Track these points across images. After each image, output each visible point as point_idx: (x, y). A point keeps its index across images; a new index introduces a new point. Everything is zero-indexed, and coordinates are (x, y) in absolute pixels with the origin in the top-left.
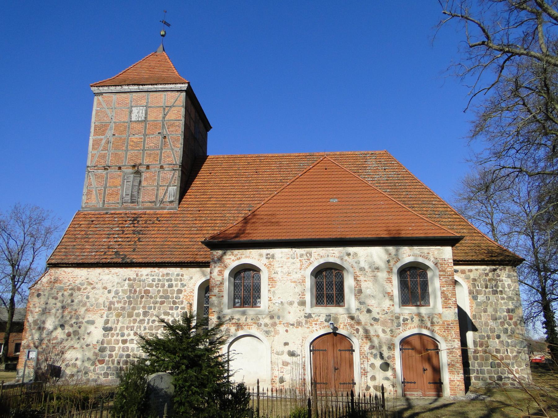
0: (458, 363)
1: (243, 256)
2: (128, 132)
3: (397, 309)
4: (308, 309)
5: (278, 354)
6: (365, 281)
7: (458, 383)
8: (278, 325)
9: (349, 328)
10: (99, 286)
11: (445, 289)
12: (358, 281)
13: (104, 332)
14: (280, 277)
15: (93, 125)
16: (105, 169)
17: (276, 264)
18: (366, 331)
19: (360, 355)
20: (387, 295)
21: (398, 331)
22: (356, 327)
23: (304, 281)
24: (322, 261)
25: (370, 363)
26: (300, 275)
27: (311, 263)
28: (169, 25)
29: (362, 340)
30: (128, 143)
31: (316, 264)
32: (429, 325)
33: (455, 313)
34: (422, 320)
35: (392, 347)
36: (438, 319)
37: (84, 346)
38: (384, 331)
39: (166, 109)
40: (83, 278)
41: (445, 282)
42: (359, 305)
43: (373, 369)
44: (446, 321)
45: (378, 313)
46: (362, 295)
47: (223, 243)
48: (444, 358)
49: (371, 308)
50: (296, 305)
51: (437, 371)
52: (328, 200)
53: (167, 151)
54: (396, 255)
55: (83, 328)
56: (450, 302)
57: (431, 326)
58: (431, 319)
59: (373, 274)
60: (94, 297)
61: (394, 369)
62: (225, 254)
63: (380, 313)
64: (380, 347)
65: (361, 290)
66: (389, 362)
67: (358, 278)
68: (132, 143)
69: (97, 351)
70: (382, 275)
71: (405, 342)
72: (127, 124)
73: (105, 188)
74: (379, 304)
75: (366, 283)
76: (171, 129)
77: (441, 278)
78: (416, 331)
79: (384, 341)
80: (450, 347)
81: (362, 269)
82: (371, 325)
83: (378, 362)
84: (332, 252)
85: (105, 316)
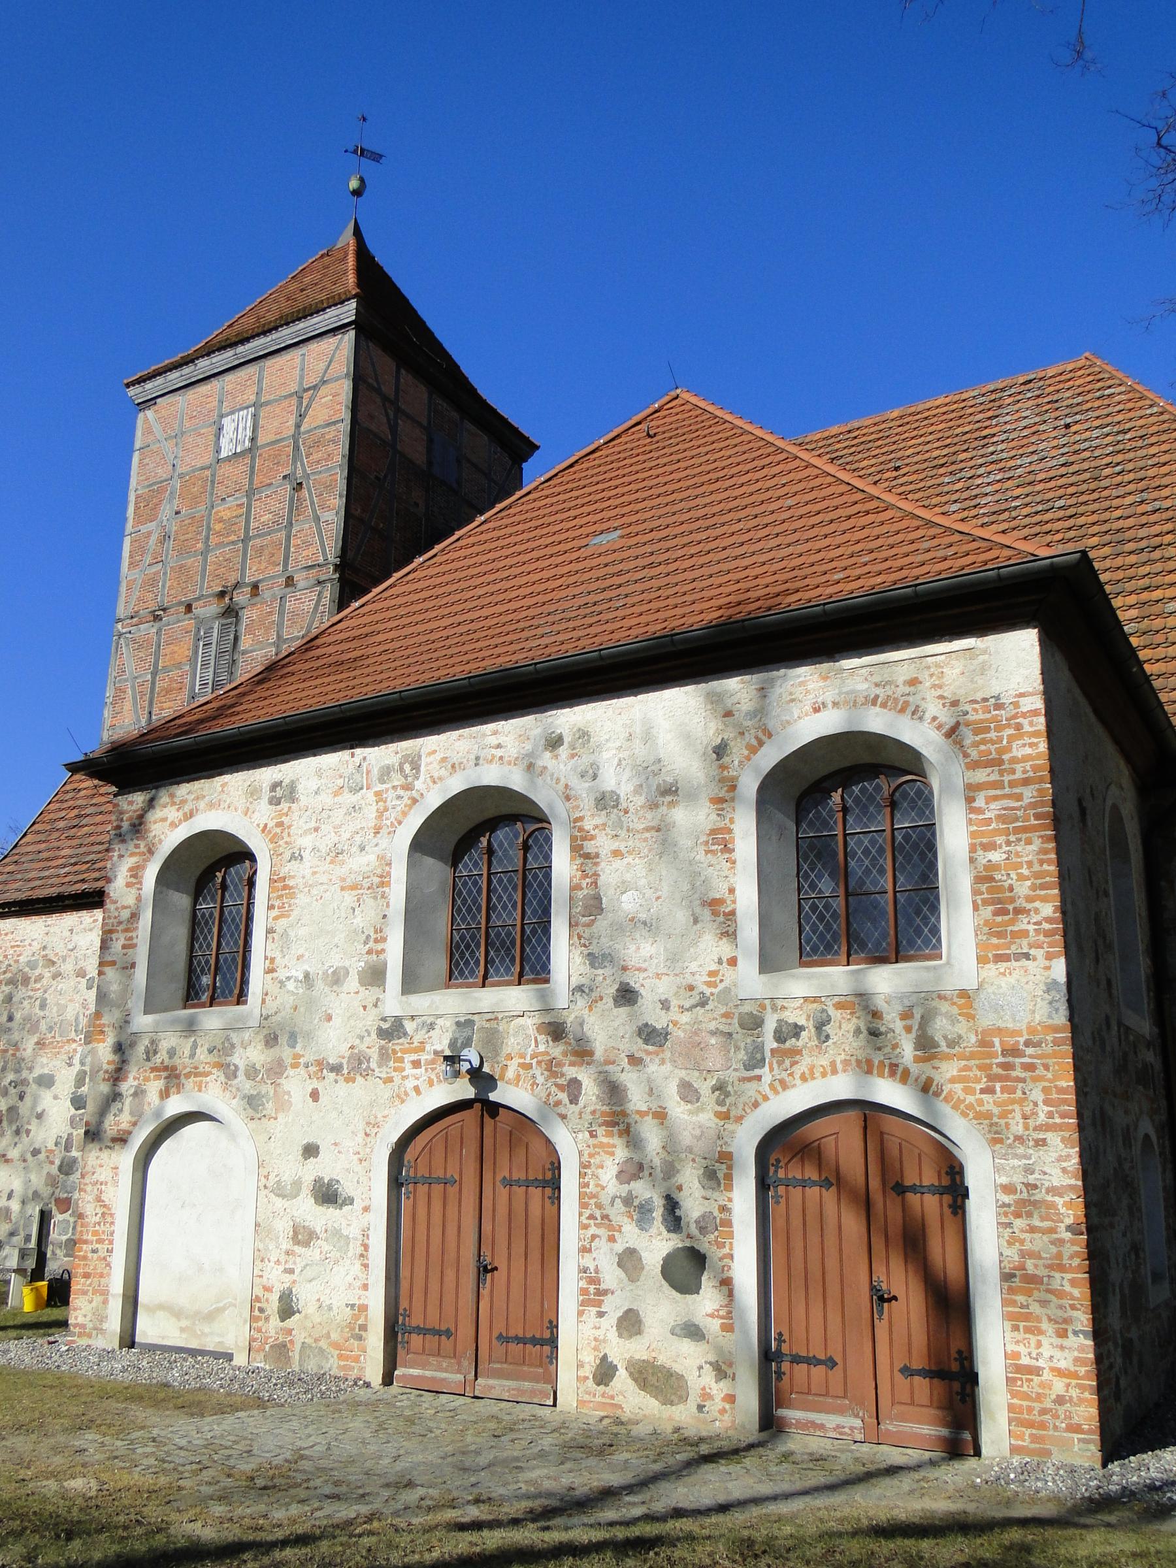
0: (1061, 1268)
1: (202, 804)
2: (212, 494)
3: (749, 980)
4: (393, 1001)
5: (280, 1191)
6: (617, 853)
7: (1059, 1386)
8: (291, 1072)
9: (540, 1080)
10: (68, 967)
11: (996, 856)
12: (587, 856)
13: (73, 1111)
14: (308, 873)
15: (132, 497)
16: (157, 618)
17: (299, 822)
18: (613, 1091)
19: (583, 1205)
20: (706, 913)
21: (751, 1089)
22: (571, 1072)
23: (384, 881)
24: (456, 785)
25: (619, 1247)
26: (372, 858)
27: (415, 801)
28: (377, 157)
29: (593, 1135)
30: (209, 528)
31: (434, 800)
32: (908, 1051)
33: (1051, 986)
34: (874, 1033)
35: (721, 1170)
36: (954, 1021)
37: (29, 1156)
38: (688, 1092)
39: (303, 396)
40: (36, 946)
41: (1000, 818)
42: (586, 969)
43: (633, 1279)
44: (1000, 1031)
45: (665, 1005)
46: (602, 924)
47: (146, 765)
48: (988, 1239)
49: (635, 980)
50: (352, 982)
51: (951, 1307)
52: (583, 542)
53: (304, 527)
54: (760, 712)
55: (28, 1099)
56: (1023, 924)
57: (917, 1059)
58: (915, 1023)
59: (650, 818)
60: (58, 1004)
61: (726, 1284)
62: (151, 804)
63: (674, 1003)
64: (670, 1170)
65: (598, 898)
66: (705, 1245)
67: (589, 847)
68: (218, 527)
69: (54, 1170)
70: (691, 818)
71: (785, 1144)
72: (208, 473)
73: (154, 674)
74: (673, 959)
75: (618, 863)
76: (315, 457)
77: (980, 802)
78: (841, 1087)
79: (686, 1138)
80: (1018, 1179)
81: (605, 801)
82: (634, 1060)
83: (657, 1245)
84: (493, 741)
85: (76, 1061)
